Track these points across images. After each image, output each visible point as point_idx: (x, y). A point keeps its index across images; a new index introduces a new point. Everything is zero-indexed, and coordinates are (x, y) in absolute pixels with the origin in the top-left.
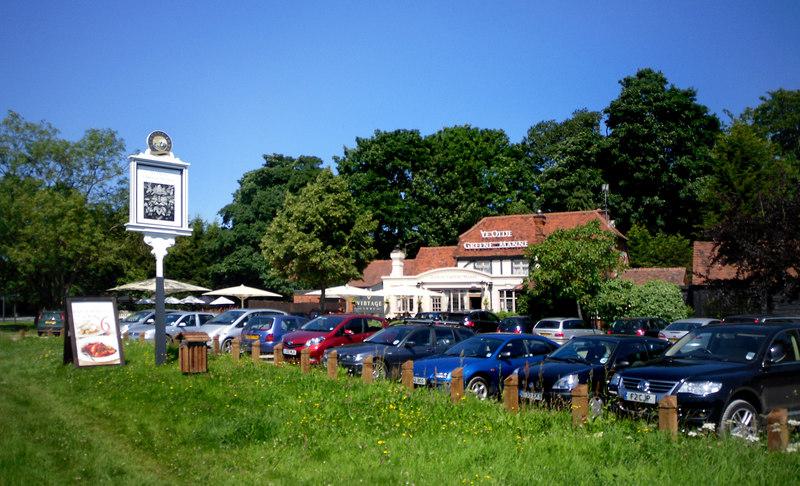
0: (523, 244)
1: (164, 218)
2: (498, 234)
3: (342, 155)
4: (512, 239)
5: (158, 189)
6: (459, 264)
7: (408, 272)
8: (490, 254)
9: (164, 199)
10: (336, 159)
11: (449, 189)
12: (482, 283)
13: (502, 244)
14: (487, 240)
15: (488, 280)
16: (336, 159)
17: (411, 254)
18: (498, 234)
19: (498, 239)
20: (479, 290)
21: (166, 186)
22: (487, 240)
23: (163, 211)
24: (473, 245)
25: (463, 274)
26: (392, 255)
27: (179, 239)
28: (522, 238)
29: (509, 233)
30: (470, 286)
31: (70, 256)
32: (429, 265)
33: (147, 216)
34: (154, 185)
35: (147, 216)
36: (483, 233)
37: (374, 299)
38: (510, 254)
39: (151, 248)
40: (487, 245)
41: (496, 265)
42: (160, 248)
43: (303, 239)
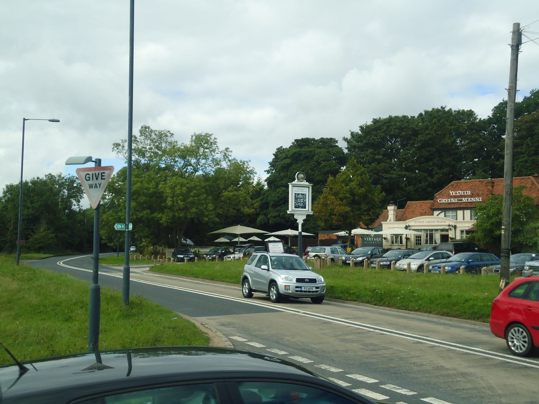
0: (479, 199)
1: (302, 208)
2: (460, 193)
3: (349, 137)
4: (472, 196)
5: (300, 196)
6: (434, 212)
7: (399, 218)
8: (456, 206)
9: (302, 200)
10: (345, 139)
11: (427, 160)
12: (449, 225)
13: (464, 200)
14: (455, 197)
15: (453, 224)
16: (345, 139)
17: (401, 206)
18: (460, 193)
19: (462, 196)
20: (447, 230)
21: (303, 194)
22: (455, 197)
23: (301, 205)
24: (444, 201)
25: (436, 220)
26: (389, 208)
27: (308, 216)
28: (478, 196)
29: (469, 193)
30: (441, 228)
31: (73, 207)
32: (414, 215)
33: (296, 207)
34: (298, 194)
35: (296, 207)
36: (451, 193)
37: (376, 236)
38: (469, 206)
39: (297, 220)
40: (453, 200)
41: (460, 213)
42: (300, 220)
43: (340, 205)
